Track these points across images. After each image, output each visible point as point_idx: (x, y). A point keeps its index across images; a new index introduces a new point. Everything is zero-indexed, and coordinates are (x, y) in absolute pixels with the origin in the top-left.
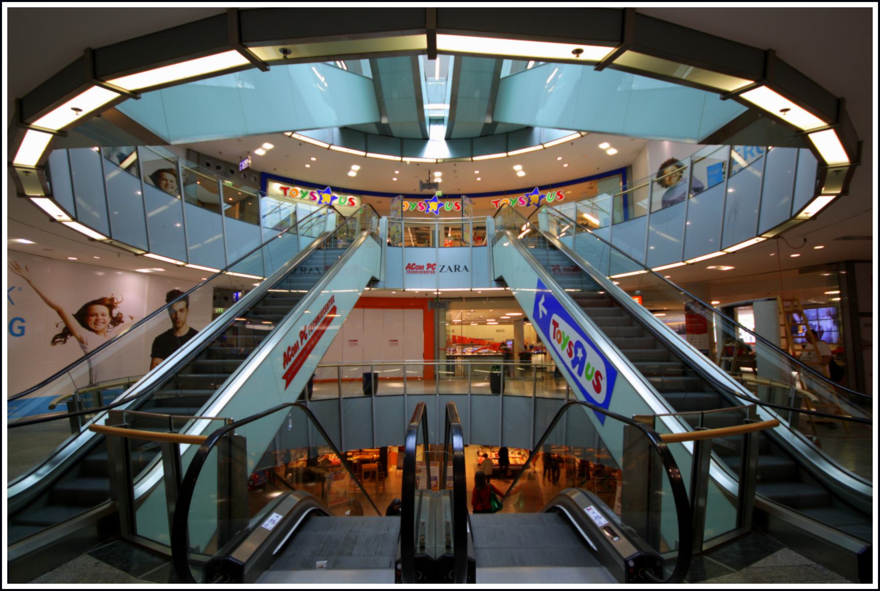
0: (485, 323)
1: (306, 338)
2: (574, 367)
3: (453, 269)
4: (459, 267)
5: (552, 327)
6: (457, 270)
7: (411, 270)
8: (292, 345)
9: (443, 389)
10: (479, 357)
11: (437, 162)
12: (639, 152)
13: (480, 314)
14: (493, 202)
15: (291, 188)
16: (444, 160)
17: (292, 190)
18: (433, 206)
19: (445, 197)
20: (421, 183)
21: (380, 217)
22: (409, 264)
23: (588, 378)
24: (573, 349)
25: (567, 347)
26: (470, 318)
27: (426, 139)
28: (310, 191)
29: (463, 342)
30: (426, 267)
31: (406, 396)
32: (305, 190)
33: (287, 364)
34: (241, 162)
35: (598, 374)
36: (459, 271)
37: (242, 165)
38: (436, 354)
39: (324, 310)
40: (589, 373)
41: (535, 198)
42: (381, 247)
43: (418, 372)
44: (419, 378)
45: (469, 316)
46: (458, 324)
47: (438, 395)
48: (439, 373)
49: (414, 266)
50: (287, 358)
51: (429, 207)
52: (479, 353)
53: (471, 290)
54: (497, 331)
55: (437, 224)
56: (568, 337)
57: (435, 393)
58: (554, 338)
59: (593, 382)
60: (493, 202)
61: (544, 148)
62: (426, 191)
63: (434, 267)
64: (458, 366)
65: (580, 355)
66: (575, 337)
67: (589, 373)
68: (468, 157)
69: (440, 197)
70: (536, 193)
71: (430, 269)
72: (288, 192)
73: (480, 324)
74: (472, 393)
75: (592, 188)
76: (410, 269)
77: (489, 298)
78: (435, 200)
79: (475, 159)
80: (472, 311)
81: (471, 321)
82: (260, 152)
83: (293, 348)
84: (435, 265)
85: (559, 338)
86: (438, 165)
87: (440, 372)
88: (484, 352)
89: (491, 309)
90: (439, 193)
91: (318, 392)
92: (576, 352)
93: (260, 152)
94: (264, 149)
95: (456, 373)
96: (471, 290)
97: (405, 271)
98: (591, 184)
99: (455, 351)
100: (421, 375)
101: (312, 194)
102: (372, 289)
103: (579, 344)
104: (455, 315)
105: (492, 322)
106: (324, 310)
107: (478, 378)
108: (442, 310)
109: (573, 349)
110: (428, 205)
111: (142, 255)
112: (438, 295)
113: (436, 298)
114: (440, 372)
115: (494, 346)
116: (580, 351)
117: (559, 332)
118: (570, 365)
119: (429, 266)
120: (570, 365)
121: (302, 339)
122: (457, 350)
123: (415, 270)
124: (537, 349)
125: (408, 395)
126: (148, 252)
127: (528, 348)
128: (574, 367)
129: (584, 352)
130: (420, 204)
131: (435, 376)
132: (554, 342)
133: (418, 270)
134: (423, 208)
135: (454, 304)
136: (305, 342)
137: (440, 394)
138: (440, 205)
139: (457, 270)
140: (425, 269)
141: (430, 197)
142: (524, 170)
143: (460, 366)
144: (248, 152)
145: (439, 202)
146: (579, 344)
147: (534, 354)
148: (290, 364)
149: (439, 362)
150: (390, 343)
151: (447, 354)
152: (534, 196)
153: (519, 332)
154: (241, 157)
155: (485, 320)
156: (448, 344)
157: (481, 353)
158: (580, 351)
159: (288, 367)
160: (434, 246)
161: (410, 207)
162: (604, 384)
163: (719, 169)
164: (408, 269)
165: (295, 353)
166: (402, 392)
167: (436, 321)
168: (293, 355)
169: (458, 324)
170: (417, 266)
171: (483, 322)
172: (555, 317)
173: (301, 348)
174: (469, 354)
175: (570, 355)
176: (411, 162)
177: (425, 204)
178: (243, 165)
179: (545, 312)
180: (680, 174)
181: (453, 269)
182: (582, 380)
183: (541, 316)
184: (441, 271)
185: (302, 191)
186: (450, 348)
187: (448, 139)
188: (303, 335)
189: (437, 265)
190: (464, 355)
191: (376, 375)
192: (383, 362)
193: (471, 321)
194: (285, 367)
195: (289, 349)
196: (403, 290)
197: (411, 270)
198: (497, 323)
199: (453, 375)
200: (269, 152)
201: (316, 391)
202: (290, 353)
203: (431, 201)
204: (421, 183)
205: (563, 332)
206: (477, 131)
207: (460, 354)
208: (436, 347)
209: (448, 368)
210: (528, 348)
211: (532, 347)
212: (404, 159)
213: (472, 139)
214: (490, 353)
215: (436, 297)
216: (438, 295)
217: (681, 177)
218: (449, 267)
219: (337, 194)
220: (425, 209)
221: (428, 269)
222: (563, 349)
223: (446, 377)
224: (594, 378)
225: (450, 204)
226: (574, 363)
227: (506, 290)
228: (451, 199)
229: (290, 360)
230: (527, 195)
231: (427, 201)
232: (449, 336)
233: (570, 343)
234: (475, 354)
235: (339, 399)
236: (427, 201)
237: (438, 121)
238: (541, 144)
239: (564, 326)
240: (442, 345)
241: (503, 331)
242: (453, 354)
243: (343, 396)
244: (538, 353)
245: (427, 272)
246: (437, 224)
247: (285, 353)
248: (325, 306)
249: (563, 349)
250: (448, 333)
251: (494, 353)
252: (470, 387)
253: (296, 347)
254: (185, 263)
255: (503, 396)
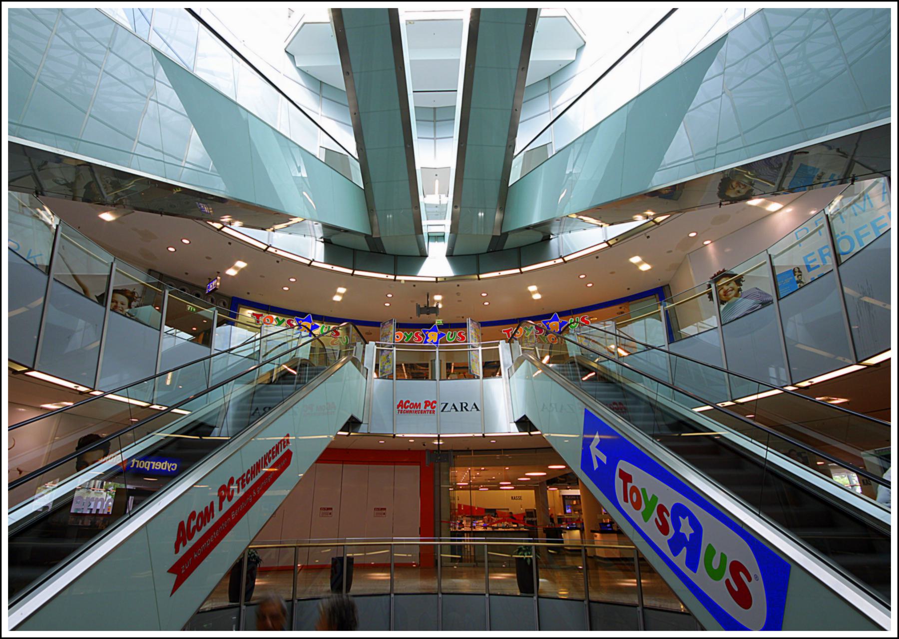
0: (498, 488)
1: (230, 499)
2: (675, 553)
3: (459, 408)
4: (467, 405)
5: (619, 482)
6: (464, 409)
7: (404, 409)
8: (199, 509)
9: (448, 583)
10: (494, 533)
11: (437, 281)
12: (678, 267)
13: (491, 473)
14: (504, 331)
15: (266, 315)
16: (445, 278)
17: (268, 317)
18: (433, 336)
19: (445, 326)
20: (418, 306)
21: (367, 343)
22: (402, 401)
23: (715, 575)
24: (669, 519)
25: (655, 514)
26: (479, 480)
27: (424, 256)
28: (287, 319)
29: (473, 513)
30: (423, 405)
31: (392, 595)
32: (281, 318)
33: (184, 545)
34: (209, 284)
35: (737, 568)
36: (467, 410)
37: (209, 287)
38: (437, 530)
39: (271, 455)
40: (716, 564)
41: (554, 325)
42: (366, 379)
43: (411, 557)
44: (414, 564)
45: (478, 476)
46: (464, 488)
47: (440, 595)
48: (441, 557)
49: (407, 404)
50: (184, 533)
51: (427, 338)
52: (493, 528)
53: (484, 436)
54: (512, 498)
55: (437, 353)
56: (654, 498)
57: (436, 591)
58: (626, 500)
59: (728, 582)
60: (504, 331)
61: (565, 262)
62: (424, 318)
63: (434, 405)
64: (466, 547)
65: (686, 529)
66: (670, 497)
67: (716, 564)
68: (474, 274)
69: (440, 327)
70: (556, 319)
71: (429, 408)
72: (261, 319)
73: (490, 489)
74: (140, 140)
75: (622, 313)
76: (402, 408)
77: (504, 450)
78: (435, 330)
79: (481, 276)
80: (483, 468)
81: (480, 484)
82: (231, 272)
83: (201, 514)
84: (435, 402)
85: (635, 500)
86: (439, 284)
87: (442, 555)
88: (501, 527)
89: (507, 466)
90: (439, 322)
91: (262, 588)
92: (677, 525)
93: (231, 272)
94: (236, 268)
95: (463, 557)
96: (484, 436)
97: (396, 410)
98: (621, 308)
99: (461, 524)
100: (416, 561)
101: (289, 322)
102: (352, 434)
103: (679, 510)
104: (462, 475)
105: (506, 486)
106: (271, 455)
107: (496, 566)
108: (444, 465)
109: (669, 519)
110: (427, 335)
111: (23, 372)
112: (439, 444)
113: (436, 451)
114: (442, 555)
115: (512, 518)
116: (685, 522)
117: (634, 489)
118: (667, 550)
119: (427, 403)
120: (667, 550)
121: (222, 499)
122: (464, 523)
123: (409, 409)
124: (569, 521)
125: (395, 594)
126: (31, 370)
127: (556, 521)
128: (675, 553)
129: (694, 523)
130: (416, 335)
131: (437, 561)
132: (627, 507)
133: (413, 409)
134: (420, 339)
135: (460, 457)
136: (227, 505)
137: (443, 594)
138: (439, 336)
139: (464, 409)
140: (422, 408)
141: (429, 326)
142: (539, 291)
143: (469, 546)
144: (218, 273)
145: (440, 332)
146: (679, 510)
147: (567, 529)
148: (190, 544)
149: (440, 540)
150: (376, 512)
151: (452, 529)
152: (553, 323)
153: (541, 497)
154: (210, 279)
155: (498, 483)
156: (453, 518)
157: (497, 528)
158: (685, 522)
159: (183, 550)
160: (433, 379)
161: (405, 337)
162: (757, 588)
163: (791, 278)
164: (400, 408)
165: (204, 523)
166: (388, 589)
167: (437, 482)
168: (198, 528)
169: (464, 488)
170: (412, 404)
171: (495, 486)
172: (623, 465)
173: (218, 515)
174: (481, 529)
175: (664, 529)
176: (406, 281)
177: (423, 335)
178: (211, 286)
179: (604, 458)
180: (739, 287)
181: (459, 408)
182: (700, 577)
183: (596, 466)
184: (442, 411)
185: (277, 318)
186: (455, 520)
187: (450, 255)
188: (224, 492)
189: (438, 403)
190: (474, 530)
191: (350, 560)
192: (321, 542)
193: (480, 484)
194: (177, 551)
195: (193, 515)
196: (392, 435)
197: (404, 409)
198: (513, 488)
199: (460, 560)
200: (242, 271)
201: (259, 586)
202: (193, 523)
203: (430, 331)
204: (418, 306)
205: (643, 490)
206: (483, 245)
207: (469, 529)
208: (437, 519)
209: (453, 549)
210: (556, 521)
211: (561, 520)
212: (398, 278)
213: (478, 255)
214: (509, 528)
215: (436, 448)
216: (439, 444)
217: (740, 290)
218: (454, 405)
219: (319, 323)
220: (423, 340)
221: (425, 408)
222: (646, 519)
223: (451, 564)
224: (728, 575)
225: (452, 335)
226: (676, 544)
227: (530, 435)
228: (453, 329)
229: (191, 537)
230: (545, 323)
231: (425, 331)
232: (454, 505)
233: (661, 509)
234: (489, 529)
235: (292, 601)
236: (425, 331)
237: (439, 237)
238: (561, 257)
239: (641, 478)
240: (446, 515)
241: (520, 498)
242: (460, 528)
243: (298, 596)
244: (571, 529)
245: (425, 412)
246: (437, 353)
247: (182, 524)
248: (273, 448)
249: (646, 519)
250: (452, 501)
251: (514, 528)
252: (488, 582)
253: (208, 513)
254: (91, 389)
255: (539, 597)
